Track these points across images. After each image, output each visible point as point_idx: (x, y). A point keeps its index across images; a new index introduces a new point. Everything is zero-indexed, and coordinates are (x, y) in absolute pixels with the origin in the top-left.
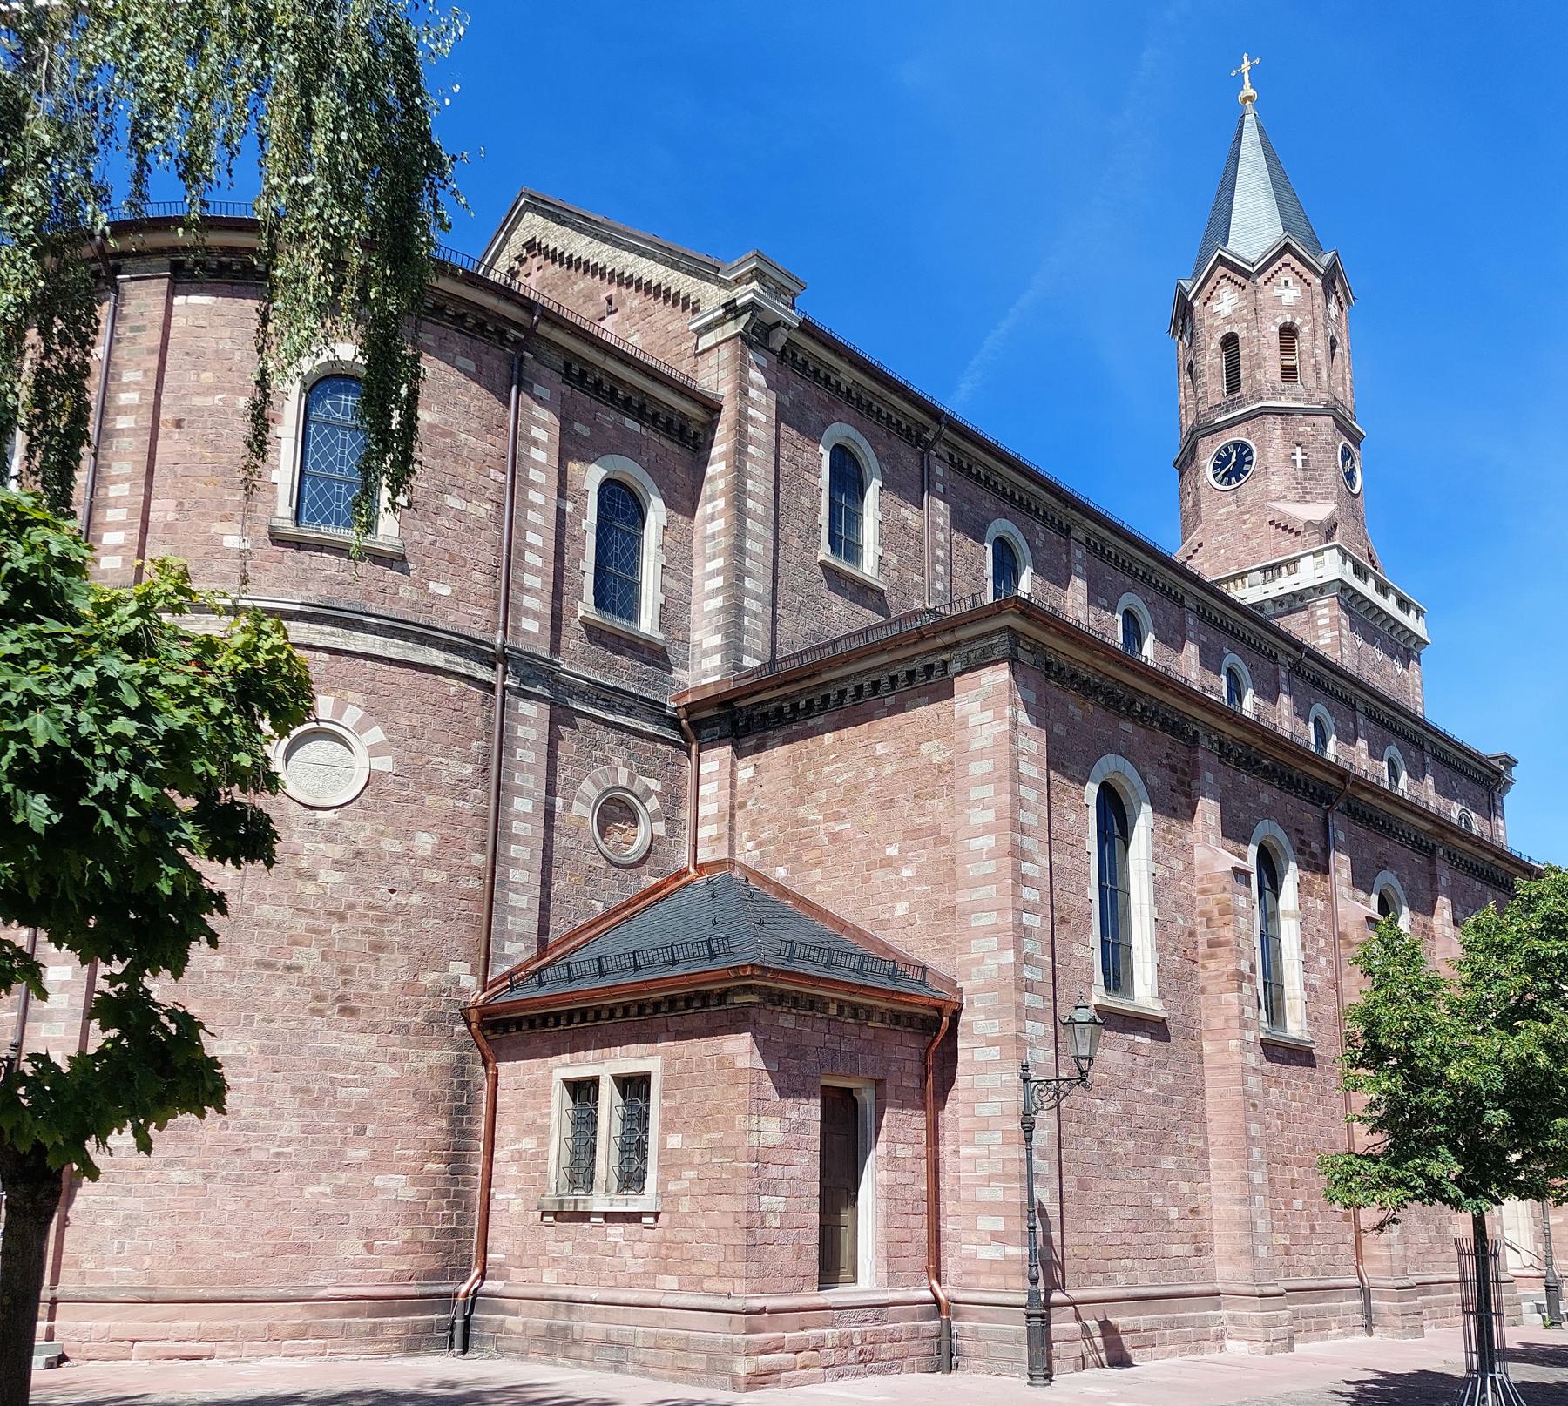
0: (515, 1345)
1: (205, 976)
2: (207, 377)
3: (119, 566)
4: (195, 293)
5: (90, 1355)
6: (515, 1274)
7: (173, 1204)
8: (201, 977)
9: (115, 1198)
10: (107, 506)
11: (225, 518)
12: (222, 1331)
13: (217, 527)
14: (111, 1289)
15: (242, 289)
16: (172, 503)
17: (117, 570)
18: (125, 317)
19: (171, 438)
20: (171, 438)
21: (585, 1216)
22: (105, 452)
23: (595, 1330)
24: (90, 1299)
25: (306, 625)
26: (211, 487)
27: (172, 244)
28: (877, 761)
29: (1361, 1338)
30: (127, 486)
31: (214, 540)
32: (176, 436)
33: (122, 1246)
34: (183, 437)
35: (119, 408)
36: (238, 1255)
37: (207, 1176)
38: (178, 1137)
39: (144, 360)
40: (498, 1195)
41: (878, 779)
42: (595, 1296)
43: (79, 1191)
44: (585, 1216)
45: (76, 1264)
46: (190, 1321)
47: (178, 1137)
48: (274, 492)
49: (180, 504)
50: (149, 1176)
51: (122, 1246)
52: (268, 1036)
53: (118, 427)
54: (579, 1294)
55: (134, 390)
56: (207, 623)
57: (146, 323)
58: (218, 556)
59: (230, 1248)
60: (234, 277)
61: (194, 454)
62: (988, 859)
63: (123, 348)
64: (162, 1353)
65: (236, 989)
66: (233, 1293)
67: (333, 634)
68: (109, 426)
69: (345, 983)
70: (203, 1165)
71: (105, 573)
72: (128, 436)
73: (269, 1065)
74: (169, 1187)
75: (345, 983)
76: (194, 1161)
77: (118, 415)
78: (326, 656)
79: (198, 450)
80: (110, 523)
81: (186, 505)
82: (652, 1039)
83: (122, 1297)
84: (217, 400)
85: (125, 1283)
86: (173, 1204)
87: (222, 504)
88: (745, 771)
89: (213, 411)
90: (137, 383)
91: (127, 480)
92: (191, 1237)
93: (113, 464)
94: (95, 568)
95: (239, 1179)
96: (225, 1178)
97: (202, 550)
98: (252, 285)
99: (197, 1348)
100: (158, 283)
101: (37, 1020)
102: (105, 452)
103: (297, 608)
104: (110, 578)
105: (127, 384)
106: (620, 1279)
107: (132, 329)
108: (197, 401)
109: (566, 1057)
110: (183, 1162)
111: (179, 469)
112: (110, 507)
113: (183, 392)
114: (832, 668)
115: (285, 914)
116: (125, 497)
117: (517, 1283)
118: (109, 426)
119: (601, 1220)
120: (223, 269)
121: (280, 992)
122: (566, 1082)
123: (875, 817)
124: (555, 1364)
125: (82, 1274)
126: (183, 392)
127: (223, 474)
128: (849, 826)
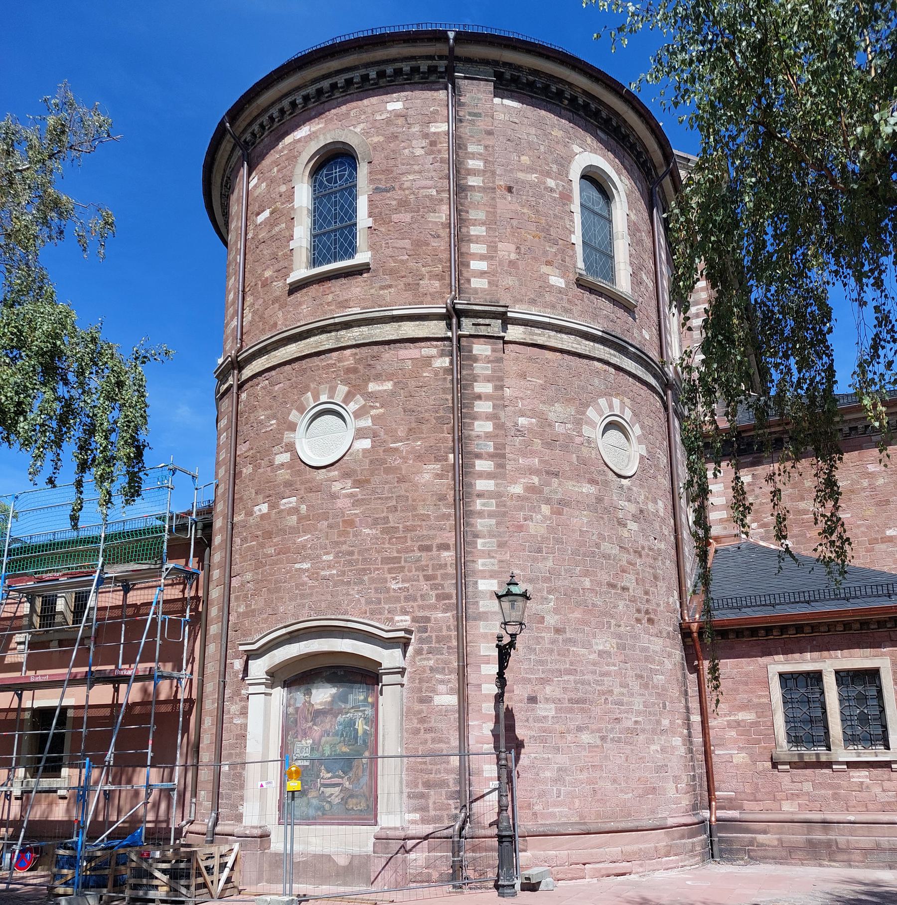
0: (770, 854)
1: (581, 592)
2: (525, 159)
3: (486, 286)
4: (508, 98)
5: (559, 876)
6: (747, 805)
7: (586, 759)
8: (579, 592)
9: (550, 756)
10: (470, 241)
11: (549, 263)
12: (634, 853)
13: (545, 269)
14: (558, 825)
15: (538, 102)
16: (512, 247)
17: (484, 290)
18: (463, 104)
19: (505, 199)
20: (505, 199)
21: (828, 765)
22: (462, 201)
23: (865, 841)
24: (549, 833)
25: (592, 344)
26: (537, 239)
27: (497, 59)
28: (871, 476)
29: (272, 837)
30: (484, 228)
31: (544, 278)
32: (510, 198)
33: (559, 791)
34: (514, 200)
35: (468, 170)
36: (626, 796)
37: (603, 739)
38: (582, 709)
39: (484, 139)
40: (718, 753)
41: (873, 488)
42: (852, 818)
43: (523, 751)
44: (828, 765)
45: (529, 806)
46: (616, 846)
47: (582, 709)
48: (573, 250)
49: (518, 248)
50: (569, 738)
51: (559, 791)
52: (620, 637)
53: (470, 184)
54: (830, 817)
55: (478, 159)
56: (549, 337)
57: (480, 111)
58: (547, 289)
59: (622, 791)
60: (535, 93)
61: (524, 213)
62: (95, 540)
63: (465, 127)
64: (604, 872)
65: (598, 601)
66: (630, 825)
67: (615, 356)
68: (462, 182)
69: (648, 601)
70: (599, 730)
71: (476, 291)
72: (479, 192)
73: (622, 657)
74: (580, 746)
75: (648, 601)
76: (594, 727)
77: (469, 175)
78: (612, 370)
79: (525, 211)
80: (474, 254)
81: (523, 250)
82: (879, 646)
83: (570, 831)
84: (533, 177)
85: (564, 820)
86: (586, 759)
87: (545, 252)
88: (746, 477)
89: (532, 185)
90: (480, 154)
91: (483, 224)
92: (601, 784)
93: (470, 211)
94: (467, 286)
95: (619, 740)
96: (612, 740)
97: (537, 284)
98: (543, 100)
99: (623, 867)
100: (487, 85)
101: (475, 619)
102: (462, 201)
103: (600, 334)
104: (480, 295)
105: (473, 154)
106: (870, 807)
107: (470, 114)
108: (521, 175)
109: (780, 657)
110: (587, 728)
111: (514, 222)
112: (472, 242)
113: (510, 167)
114: (851, 413)
115: (615, 551)
116: (484, 236)
117: (752, 812)
118: (462, 182)
119: (845, 767)
120: (531, 85)
121: (621, 605)
122: (781, 675)
123: (873, 511)
124: (820, 865)
125: (535, 814)
126: (510, 167)
127: (543, 231)
128: (849, 515)
